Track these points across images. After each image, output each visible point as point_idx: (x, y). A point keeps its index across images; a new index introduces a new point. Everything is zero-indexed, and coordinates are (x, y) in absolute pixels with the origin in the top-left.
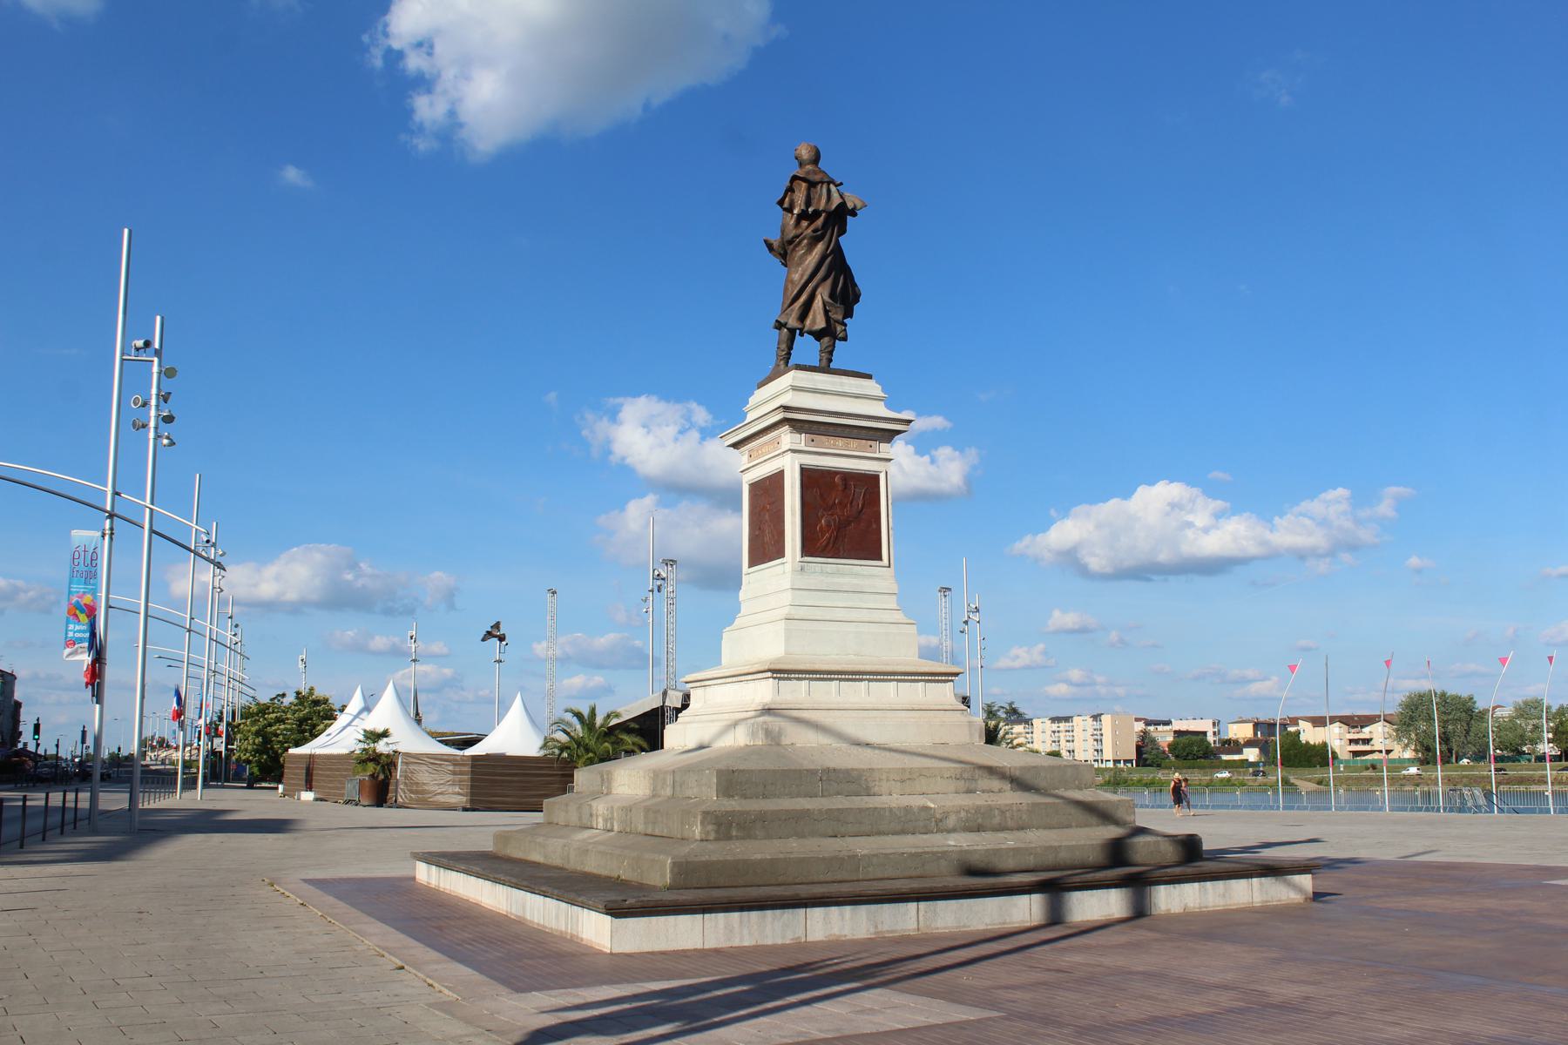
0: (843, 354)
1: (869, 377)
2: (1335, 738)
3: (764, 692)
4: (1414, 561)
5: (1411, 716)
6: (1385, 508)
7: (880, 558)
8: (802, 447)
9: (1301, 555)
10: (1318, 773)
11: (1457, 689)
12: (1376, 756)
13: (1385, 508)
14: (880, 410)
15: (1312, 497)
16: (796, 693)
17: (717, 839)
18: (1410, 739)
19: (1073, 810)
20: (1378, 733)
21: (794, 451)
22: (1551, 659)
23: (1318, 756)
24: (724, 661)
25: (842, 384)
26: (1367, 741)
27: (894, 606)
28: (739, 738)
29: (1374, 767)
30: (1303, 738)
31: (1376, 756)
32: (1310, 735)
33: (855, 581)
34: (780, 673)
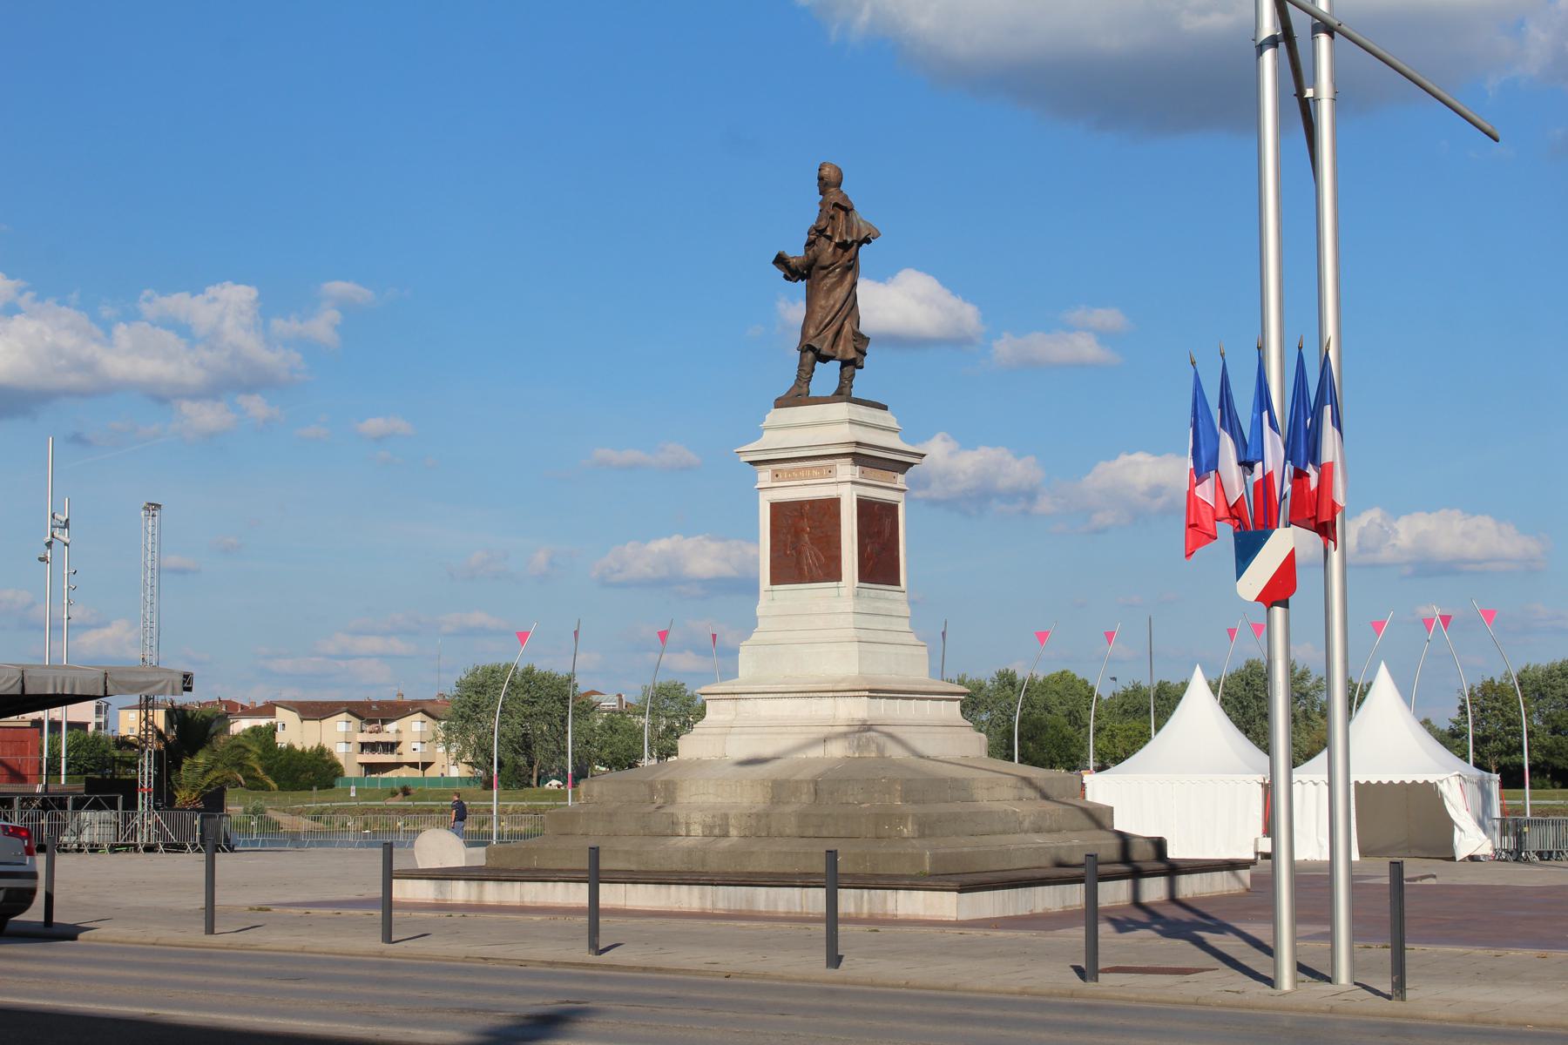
0: (862, 384)
1: (885, 408)
2: (338, 737)
3: (856, 709)
4: (374, 425)
5: (464, 712)
6: (323, 326)
8: (857, 478)
9: (161, 397)
10: (315, 800)
12: (405, 773)
13: (323, 326)
14: (893, 441)
15: (196, 290)
16: (883, 709)
18: (465, 744)
19: (1079, 813)
20: (412, 733)
21: (853, 483)
23: (316, 771)
24: (743, 672)
26: (391, 747)
28: (837, 750)
29: (406, 792)
30: (282, 739)
31: (405, 773)
32: (295, 733)
34: (875, 693)
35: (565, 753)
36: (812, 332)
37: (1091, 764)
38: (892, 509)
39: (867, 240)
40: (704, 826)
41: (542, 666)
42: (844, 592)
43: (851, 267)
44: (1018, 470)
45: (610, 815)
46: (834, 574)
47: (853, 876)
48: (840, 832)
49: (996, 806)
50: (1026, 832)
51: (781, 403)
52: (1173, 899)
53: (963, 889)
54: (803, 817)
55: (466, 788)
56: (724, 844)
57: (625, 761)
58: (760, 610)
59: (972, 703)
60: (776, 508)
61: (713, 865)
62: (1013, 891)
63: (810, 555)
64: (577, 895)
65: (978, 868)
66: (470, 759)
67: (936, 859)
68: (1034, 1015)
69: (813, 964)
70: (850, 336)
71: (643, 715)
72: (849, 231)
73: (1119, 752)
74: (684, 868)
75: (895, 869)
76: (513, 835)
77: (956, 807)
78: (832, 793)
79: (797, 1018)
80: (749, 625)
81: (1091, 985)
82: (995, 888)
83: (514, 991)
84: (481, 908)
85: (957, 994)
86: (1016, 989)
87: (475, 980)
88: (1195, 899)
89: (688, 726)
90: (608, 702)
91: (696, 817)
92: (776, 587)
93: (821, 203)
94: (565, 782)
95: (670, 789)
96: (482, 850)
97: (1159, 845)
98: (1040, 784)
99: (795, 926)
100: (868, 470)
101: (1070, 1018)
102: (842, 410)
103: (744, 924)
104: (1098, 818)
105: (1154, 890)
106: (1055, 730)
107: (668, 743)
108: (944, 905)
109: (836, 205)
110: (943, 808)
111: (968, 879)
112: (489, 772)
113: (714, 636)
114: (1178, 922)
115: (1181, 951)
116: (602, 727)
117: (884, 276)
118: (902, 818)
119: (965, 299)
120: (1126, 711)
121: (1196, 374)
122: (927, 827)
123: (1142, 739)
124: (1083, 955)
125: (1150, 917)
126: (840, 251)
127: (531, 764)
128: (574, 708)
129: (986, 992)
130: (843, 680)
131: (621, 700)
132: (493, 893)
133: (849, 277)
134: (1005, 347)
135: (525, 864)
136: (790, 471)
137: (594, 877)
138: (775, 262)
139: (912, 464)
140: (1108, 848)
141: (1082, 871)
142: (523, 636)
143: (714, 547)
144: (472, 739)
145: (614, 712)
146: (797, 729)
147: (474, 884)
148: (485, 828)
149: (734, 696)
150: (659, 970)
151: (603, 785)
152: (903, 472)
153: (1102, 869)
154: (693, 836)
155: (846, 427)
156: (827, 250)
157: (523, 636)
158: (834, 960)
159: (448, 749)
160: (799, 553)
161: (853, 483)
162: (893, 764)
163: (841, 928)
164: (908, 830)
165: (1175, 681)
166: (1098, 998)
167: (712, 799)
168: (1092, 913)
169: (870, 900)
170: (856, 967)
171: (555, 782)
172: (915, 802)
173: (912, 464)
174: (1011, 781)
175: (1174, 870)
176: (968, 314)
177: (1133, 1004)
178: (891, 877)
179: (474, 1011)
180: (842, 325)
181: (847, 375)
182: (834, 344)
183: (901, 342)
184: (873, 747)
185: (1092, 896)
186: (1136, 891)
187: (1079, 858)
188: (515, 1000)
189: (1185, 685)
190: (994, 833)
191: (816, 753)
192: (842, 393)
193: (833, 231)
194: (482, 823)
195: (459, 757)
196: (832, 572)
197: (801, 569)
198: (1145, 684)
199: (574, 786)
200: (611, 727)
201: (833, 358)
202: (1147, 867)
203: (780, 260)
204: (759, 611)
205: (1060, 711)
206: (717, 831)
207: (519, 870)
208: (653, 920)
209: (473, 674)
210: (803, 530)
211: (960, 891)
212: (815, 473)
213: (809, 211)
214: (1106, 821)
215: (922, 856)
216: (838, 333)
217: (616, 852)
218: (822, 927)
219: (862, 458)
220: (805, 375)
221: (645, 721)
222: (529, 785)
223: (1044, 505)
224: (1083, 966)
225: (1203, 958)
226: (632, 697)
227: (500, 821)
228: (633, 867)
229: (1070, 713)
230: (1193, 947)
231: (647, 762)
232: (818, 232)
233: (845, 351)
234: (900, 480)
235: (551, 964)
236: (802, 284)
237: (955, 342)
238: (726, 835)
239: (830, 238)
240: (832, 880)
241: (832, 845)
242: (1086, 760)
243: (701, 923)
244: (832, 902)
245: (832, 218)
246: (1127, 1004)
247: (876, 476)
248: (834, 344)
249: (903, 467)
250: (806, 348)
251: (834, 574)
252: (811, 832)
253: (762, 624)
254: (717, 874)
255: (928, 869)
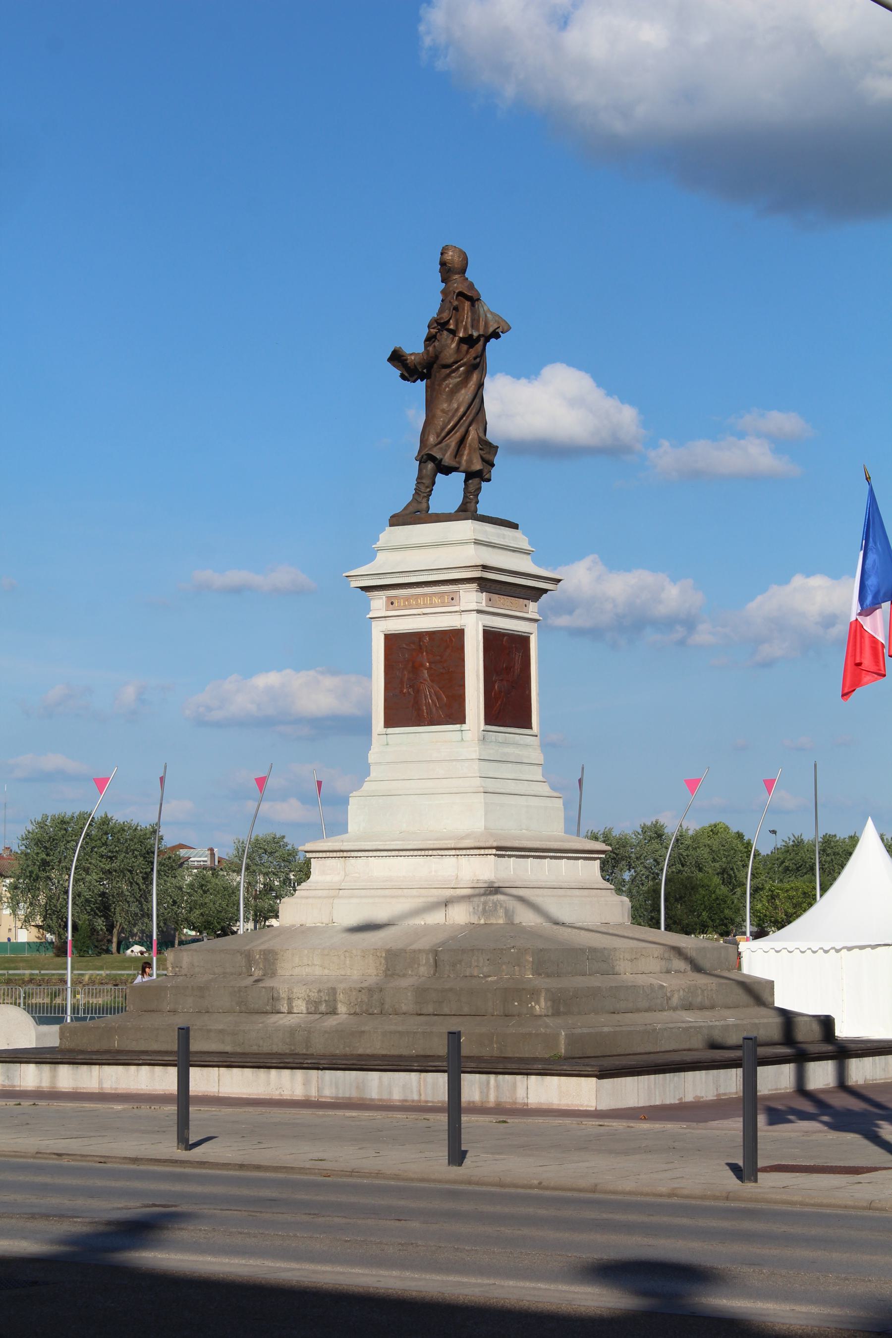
0: (489, 499)
1: (515, 526)
3: (484, 869)
7: (529, 726)
8: (483, 606)
11: (130, 811)
17: (553, 1015)
19: (740, 991)
21: (479, 612)
22: (774, 832)
24: (353, 826)
25: (504, 536)
27: (540, 778)
28: (460, 916)
33: (517, 751)
34: (503, 850)
35: (150, 916)
36: (432, 439)
37: (748, 929)
38: (523, 641)
39: (496, 335)
40: (308, 1002)
41: (119, 816)
42: (468, 736)
43: (478, 366)
44: (673, 595)
45: (201, 989)
46: (457, 716)
47: (479, 1059)
48: (467, 1007)
49: (641, 980)
50: (675, 1009)
51: (397, 520)
52: (842, 1085)
53: (603, 1074)
54: (421, 992)
55: (36, 955)
56: (331, 1022)
57: (219, 926)
58: (373, 756)
59: (615, 860)
60: (392, 641)
61: (319, 1046)
62: (660, 1077)
63: (429, 693)
64: (165, 1080)
65: (620, 1051)
66: (39, 921)
67: (572, 1040)
68: (685, 1221)
69: (428, 1161)
70: (476, 444)
71: (239, 872)
72: (475, 323)
73: (781, 916)
74: (285, 1049)
75: (526, 1051)
76: (88, 1009)
77: (596, 981)
78: (454, 965)
79: (415, 1225)
80: (361, 771)
81: (749, 1185)
82: (664, 1071)
83: (91, 1193)
84: (54, 1095)
85: (597, 1196)
86: (663, 1189)
87: (47, 1179)
88: (866, 1086)
89: (289, 886)
90: (199, 857)
91: (300, 992)
92: (390, 730)
93: (443, 292)
94: (149, 948)
95: (270, 959)
96: (55, 1028)
97: (827, 1023)
98: (693, 954)
99: (413, 1116)
100: (495, 597)
101: (726, 1224)
102: (466, 528)
103: (354, 1114)
104: (757, 993)
105: (821, 1075)
106: (709, 890)
107: (265, 904)
108: (581, 1092)
109: (460, 294)
110: (580, 982)
111: (607, 1063)
112: (61, 936)
113: (319, 783)
114: (849, 1113)
115: (852, 1146)
116: (191, 886)
117: (527, 369)
118: (534, 994)
119: (623, 400)
120: (787, 869)
121: (871, 491)
122: (561, 1004)
123: (805, 901)
124: (740, 1151)
125: (810, 1104)
126: (464, 347)
127: (110, 928)
128: (160, 864)
129: (630, 1193)
130: (467, 836)
131: (213, 855)
132: (68, 1078)
133: (475, 377)
134: (666, 457)
135: (104, 1045)
136: (407, 598)
137: (184, 1059)
138: (390, 360)
139: (545, 591)
140: (769, 1028)
141: (738, 1054)
142: (101, 783)
143: (329, 682)
144: (42, 899)
145: (205, 868)
146: (414, 892)
147: (46, 1068)
148: (58, 1001)
149: (343, 853)
150: (258, 1168)
151: (194, 958)
152: (535, 599)
153: (762, 1051)
154: (295, 1014)
155: (471, 549)
156: (450, 346)
157: (101, 783)
158: (457, 1156)
159: (14, 913)
160: (417, 691)
161: (479, 612)
162: (522, 931)
163: (464, 1118)
164: (540, 1007)
165: (842, 834)
166: (757, 1200)
167: (318, 971)
168: (750, 1102)
169: (497, 1087)
170: (481, 1165)
171: (137, 948)
172: (548, 976)
173: (545, 591)
174: (657, 951)
175: (843, 1052)
176: (626, 417)
177: (798, 1208)
178: (521, 1060)
179: (46, 1216)
180: (467, 432)
181: (472, 488)
182: (458, 453)
183: (547, 450)
184: (501, 912)
185: (750, 1082)
186: (801, 1077)
187: (734, 1039)
188: (599, 1238)
189: (854, 841)
190: (638, 1010)
191: (436, 918)
192: (467, 510)
193: (457, 325)
194: (55, 995)
195: (27, 920)
196: (455, 714)
197: (419, 710)
198: (808, 836)
199: (159, 952)
200: (202, 885)
201: (456, 469)
202: (813, 1049)
203: (397, 358)
204: (372, 757)
205: (712, 868)
206: (323, 1008)
207: (97, 1052)
208: (250, 1109)
209: (42, 825)
210: (422, 665)
211: (600, 1076)
212: (436, 600)
213: (428, 300)
214: (765, 996)
215: (556, 1036)
216: (462, 441)
217: (209, 1031)
218: (443, 1118)
219: (490, 584)
220: (424, 488)
221: (240, 879)
222: (108, 951)
223: (704, 635)
224: (741, 1163)
225: (873, 1154)
226: (226, 851)
227: (74, 993)
228: (228, 1049)
229: (723, 871)
230: (866, 1142)
231: (243, 926)
232: (439, 326)
233: (470, 461)
234: (532, 609)
235: (135, 1160)
236: (421, 385)
237: (610, 451)
238: (334, 1012)
239: (453, 332)
240: (455, 1063)
241: (454, 1025)
242: (740, 926)
243: (306, 1112)
244: (455, 1089)
245: (456, 309)
246: (790, 1208)
247: (505, 604)
248: (458, 453)
249: (535, 594)
250: (425, 458)
251: (457, 716)
252: (430, 1009)
253: (374, 773)
254: (324, 1056)
255: (563, 1051)
